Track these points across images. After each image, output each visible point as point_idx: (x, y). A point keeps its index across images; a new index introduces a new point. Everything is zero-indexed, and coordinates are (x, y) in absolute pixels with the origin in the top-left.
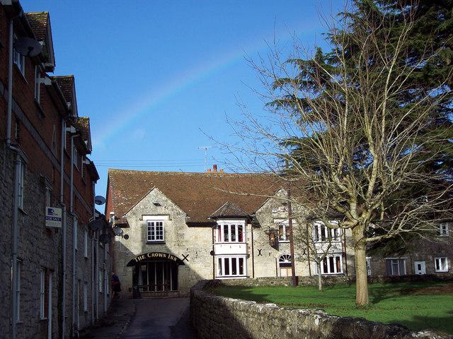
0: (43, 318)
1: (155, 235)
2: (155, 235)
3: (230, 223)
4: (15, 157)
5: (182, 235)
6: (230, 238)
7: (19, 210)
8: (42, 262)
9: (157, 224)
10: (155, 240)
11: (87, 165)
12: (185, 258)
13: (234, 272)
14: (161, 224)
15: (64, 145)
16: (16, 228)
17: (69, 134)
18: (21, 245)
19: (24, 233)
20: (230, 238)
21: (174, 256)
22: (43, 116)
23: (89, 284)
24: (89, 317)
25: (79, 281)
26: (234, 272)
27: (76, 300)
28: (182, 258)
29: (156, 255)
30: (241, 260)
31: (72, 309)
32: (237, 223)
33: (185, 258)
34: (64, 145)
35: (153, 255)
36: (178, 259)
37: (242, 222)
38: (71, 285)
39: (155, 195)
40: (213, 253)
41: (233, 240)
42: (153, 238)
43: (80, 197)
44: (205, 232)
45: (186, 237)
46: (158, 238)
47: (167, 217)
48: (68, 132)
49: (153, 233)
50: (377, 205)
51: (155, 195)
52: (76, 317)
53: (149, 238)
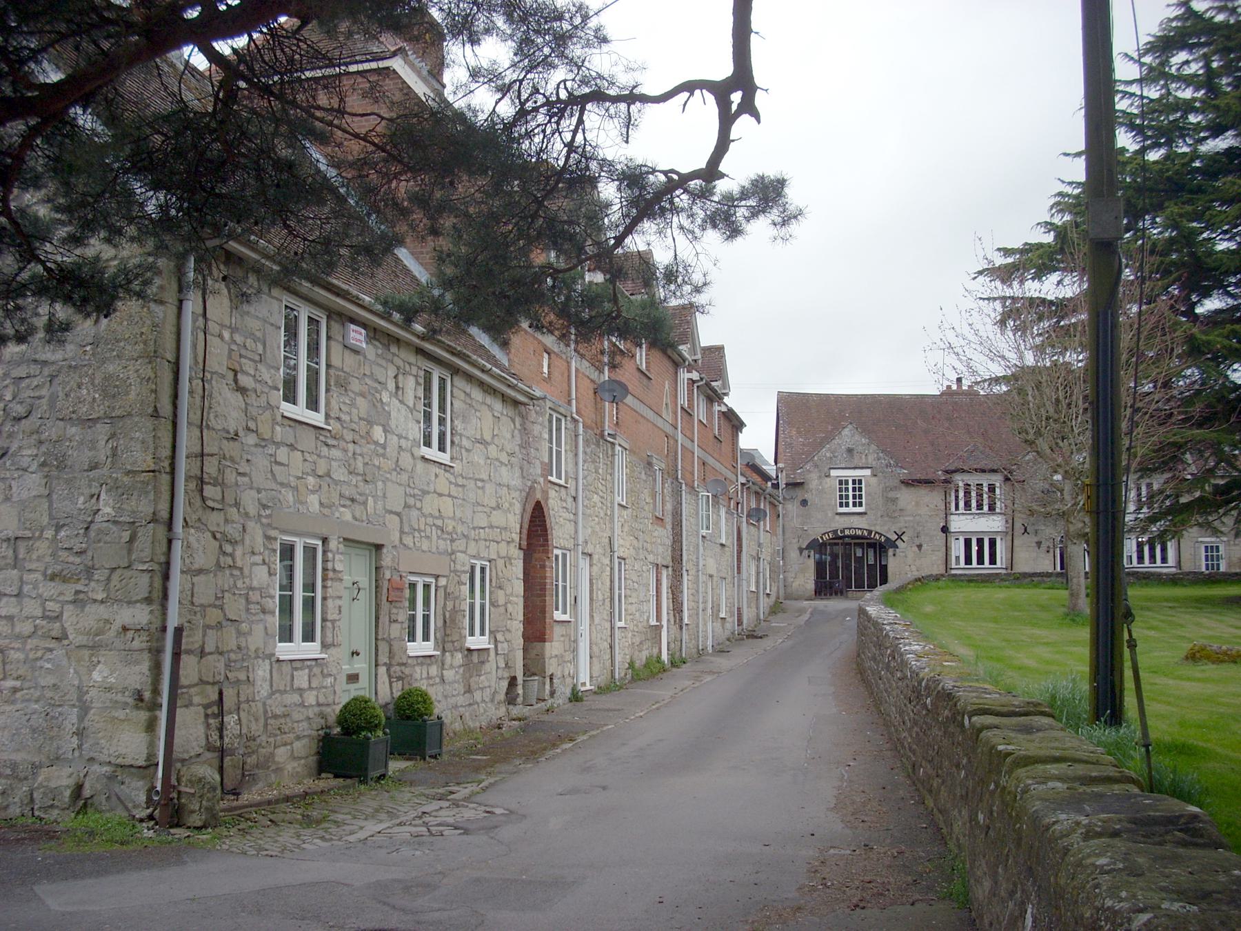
0: (653, 622)
2: (851, 501)
4: (613, 449)
6: (974, 504)
8: (651, 558)
9: (854, 482)
10: (851, 509)
12: (899, 537)
13: (980, 560)
15: (683, 400)
16: (617, 526)
18: (621, 542)
19: (626, 529)
20: (974, 504)
21: (881, 535)
22: (650, 379)
23: (729, 579)
24: (728, 626)
25: (711, 576)
26: (980, 560)
27: (705, 602)
29: (852, 532)
30: (993, 543)
32: (985, 480)
33: (899, 537)
34: (683, 400)
35: (847, 532)
37: (997, 479)
38: (697, 582)
39: (848, 436)
41: (980, 506)
42: (847, 505)
43: (710, 461)
44: (930, 500)
46: (854, 505)
47: (868, 472)
49: (847, 497)
50: (1144, 489)
51: (848, 436)
53: (841, 505)
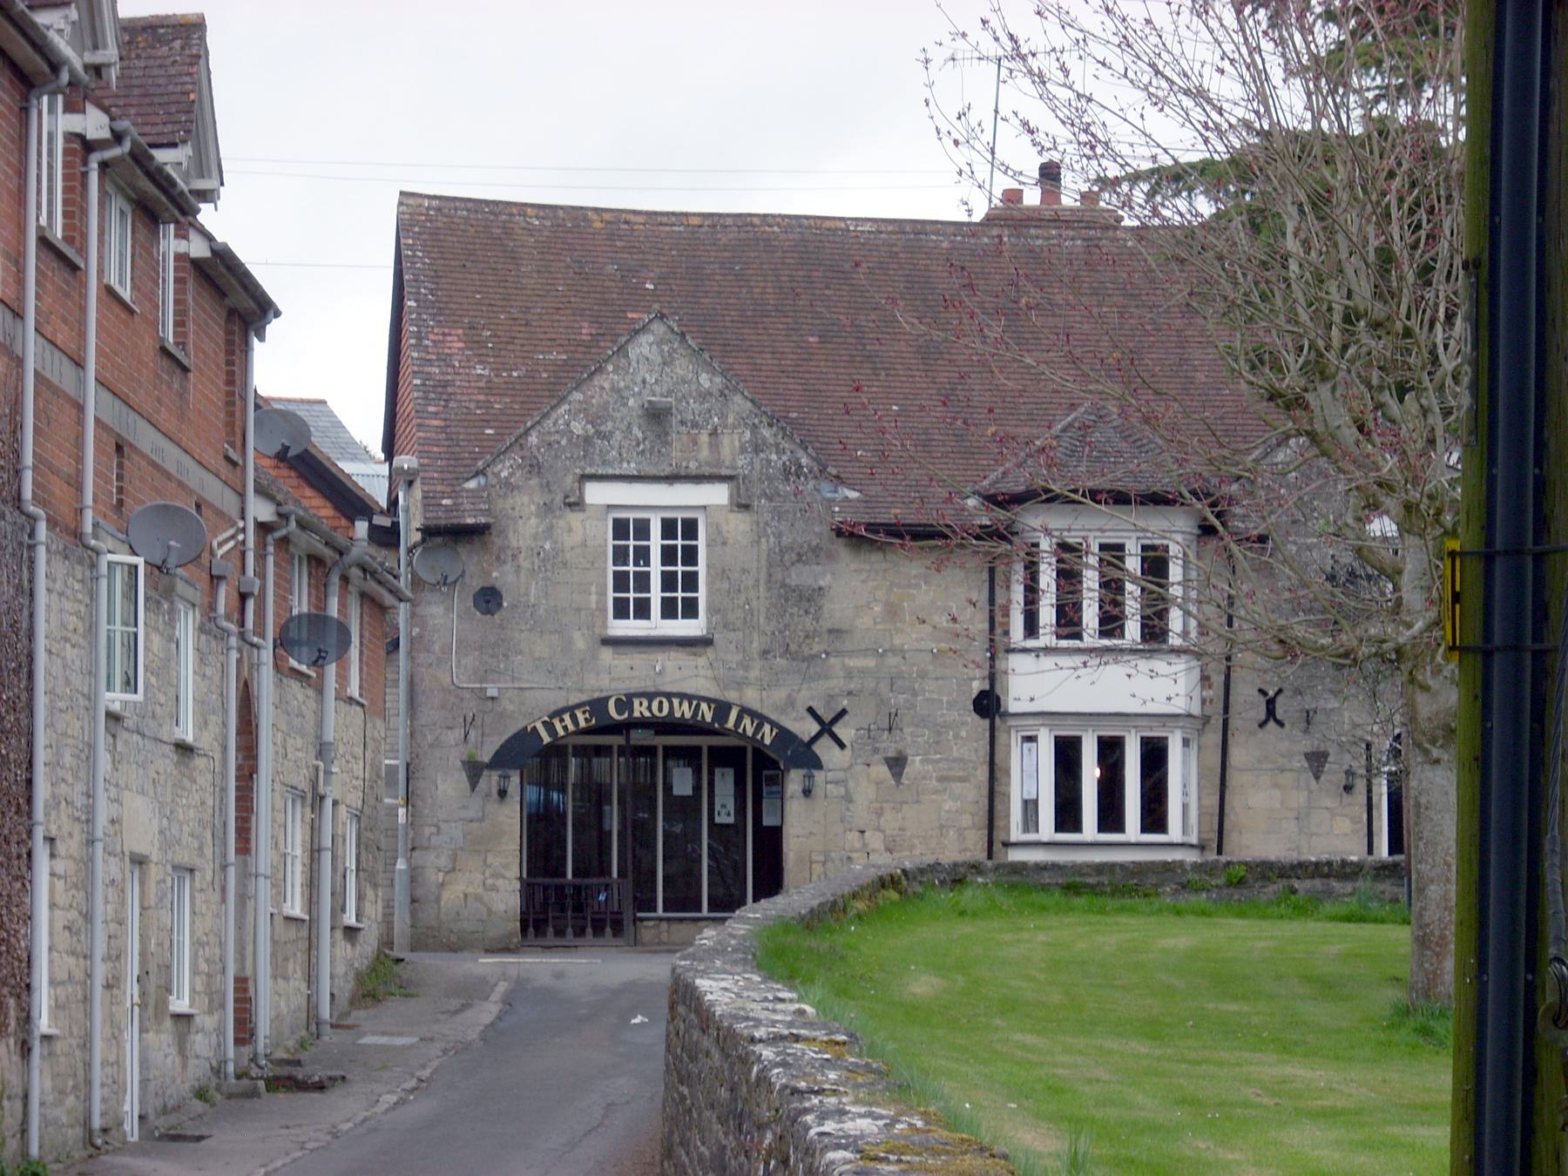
1: (656, 595)
2: (656, 595)
3: (1092, 528)
5: (810, 598)
6: (1090, 616)
7: (44, 242)
9: (668, 528)
11: (197, 264)
12: (826, 728)
13: (1111, 817)
14: (690, 528)
17: (83, 146)
20: (1090, 616)
21: (760, 719)
23: (207, 872)
24: (200, 1043)
25: (139, 861)
26: (1111, 817)
27: (115, 957)
28: (806, 728)
30: (1154, 756)
31: (87, 1000)
32: (1133, 532)
33: (826, 728)
35: (640, 709)
36: (784, 736)
37: (1173, 531)
38: (84, 882)
39: (650, 363)
40: (988, 704)
42: (643, 610)
43: (146, 438)
45: (837, 609)
47: (717, 495)
48: (71, 137)
49: (643, 581)
52: (115, 1038)
53: (621, 611)
